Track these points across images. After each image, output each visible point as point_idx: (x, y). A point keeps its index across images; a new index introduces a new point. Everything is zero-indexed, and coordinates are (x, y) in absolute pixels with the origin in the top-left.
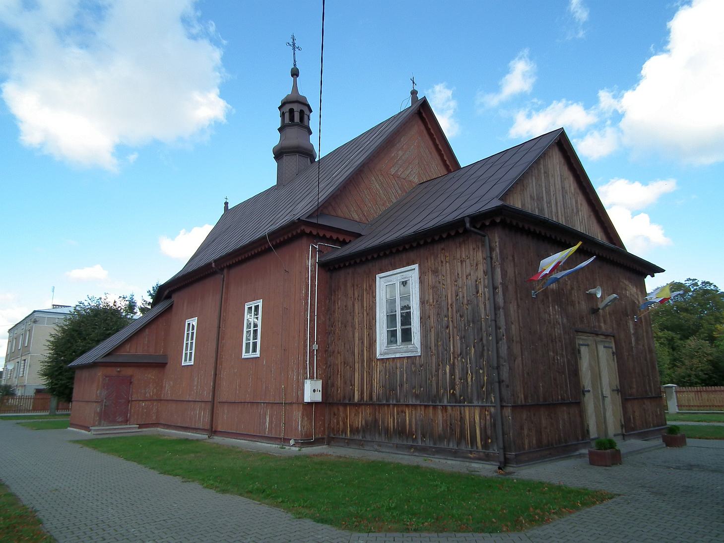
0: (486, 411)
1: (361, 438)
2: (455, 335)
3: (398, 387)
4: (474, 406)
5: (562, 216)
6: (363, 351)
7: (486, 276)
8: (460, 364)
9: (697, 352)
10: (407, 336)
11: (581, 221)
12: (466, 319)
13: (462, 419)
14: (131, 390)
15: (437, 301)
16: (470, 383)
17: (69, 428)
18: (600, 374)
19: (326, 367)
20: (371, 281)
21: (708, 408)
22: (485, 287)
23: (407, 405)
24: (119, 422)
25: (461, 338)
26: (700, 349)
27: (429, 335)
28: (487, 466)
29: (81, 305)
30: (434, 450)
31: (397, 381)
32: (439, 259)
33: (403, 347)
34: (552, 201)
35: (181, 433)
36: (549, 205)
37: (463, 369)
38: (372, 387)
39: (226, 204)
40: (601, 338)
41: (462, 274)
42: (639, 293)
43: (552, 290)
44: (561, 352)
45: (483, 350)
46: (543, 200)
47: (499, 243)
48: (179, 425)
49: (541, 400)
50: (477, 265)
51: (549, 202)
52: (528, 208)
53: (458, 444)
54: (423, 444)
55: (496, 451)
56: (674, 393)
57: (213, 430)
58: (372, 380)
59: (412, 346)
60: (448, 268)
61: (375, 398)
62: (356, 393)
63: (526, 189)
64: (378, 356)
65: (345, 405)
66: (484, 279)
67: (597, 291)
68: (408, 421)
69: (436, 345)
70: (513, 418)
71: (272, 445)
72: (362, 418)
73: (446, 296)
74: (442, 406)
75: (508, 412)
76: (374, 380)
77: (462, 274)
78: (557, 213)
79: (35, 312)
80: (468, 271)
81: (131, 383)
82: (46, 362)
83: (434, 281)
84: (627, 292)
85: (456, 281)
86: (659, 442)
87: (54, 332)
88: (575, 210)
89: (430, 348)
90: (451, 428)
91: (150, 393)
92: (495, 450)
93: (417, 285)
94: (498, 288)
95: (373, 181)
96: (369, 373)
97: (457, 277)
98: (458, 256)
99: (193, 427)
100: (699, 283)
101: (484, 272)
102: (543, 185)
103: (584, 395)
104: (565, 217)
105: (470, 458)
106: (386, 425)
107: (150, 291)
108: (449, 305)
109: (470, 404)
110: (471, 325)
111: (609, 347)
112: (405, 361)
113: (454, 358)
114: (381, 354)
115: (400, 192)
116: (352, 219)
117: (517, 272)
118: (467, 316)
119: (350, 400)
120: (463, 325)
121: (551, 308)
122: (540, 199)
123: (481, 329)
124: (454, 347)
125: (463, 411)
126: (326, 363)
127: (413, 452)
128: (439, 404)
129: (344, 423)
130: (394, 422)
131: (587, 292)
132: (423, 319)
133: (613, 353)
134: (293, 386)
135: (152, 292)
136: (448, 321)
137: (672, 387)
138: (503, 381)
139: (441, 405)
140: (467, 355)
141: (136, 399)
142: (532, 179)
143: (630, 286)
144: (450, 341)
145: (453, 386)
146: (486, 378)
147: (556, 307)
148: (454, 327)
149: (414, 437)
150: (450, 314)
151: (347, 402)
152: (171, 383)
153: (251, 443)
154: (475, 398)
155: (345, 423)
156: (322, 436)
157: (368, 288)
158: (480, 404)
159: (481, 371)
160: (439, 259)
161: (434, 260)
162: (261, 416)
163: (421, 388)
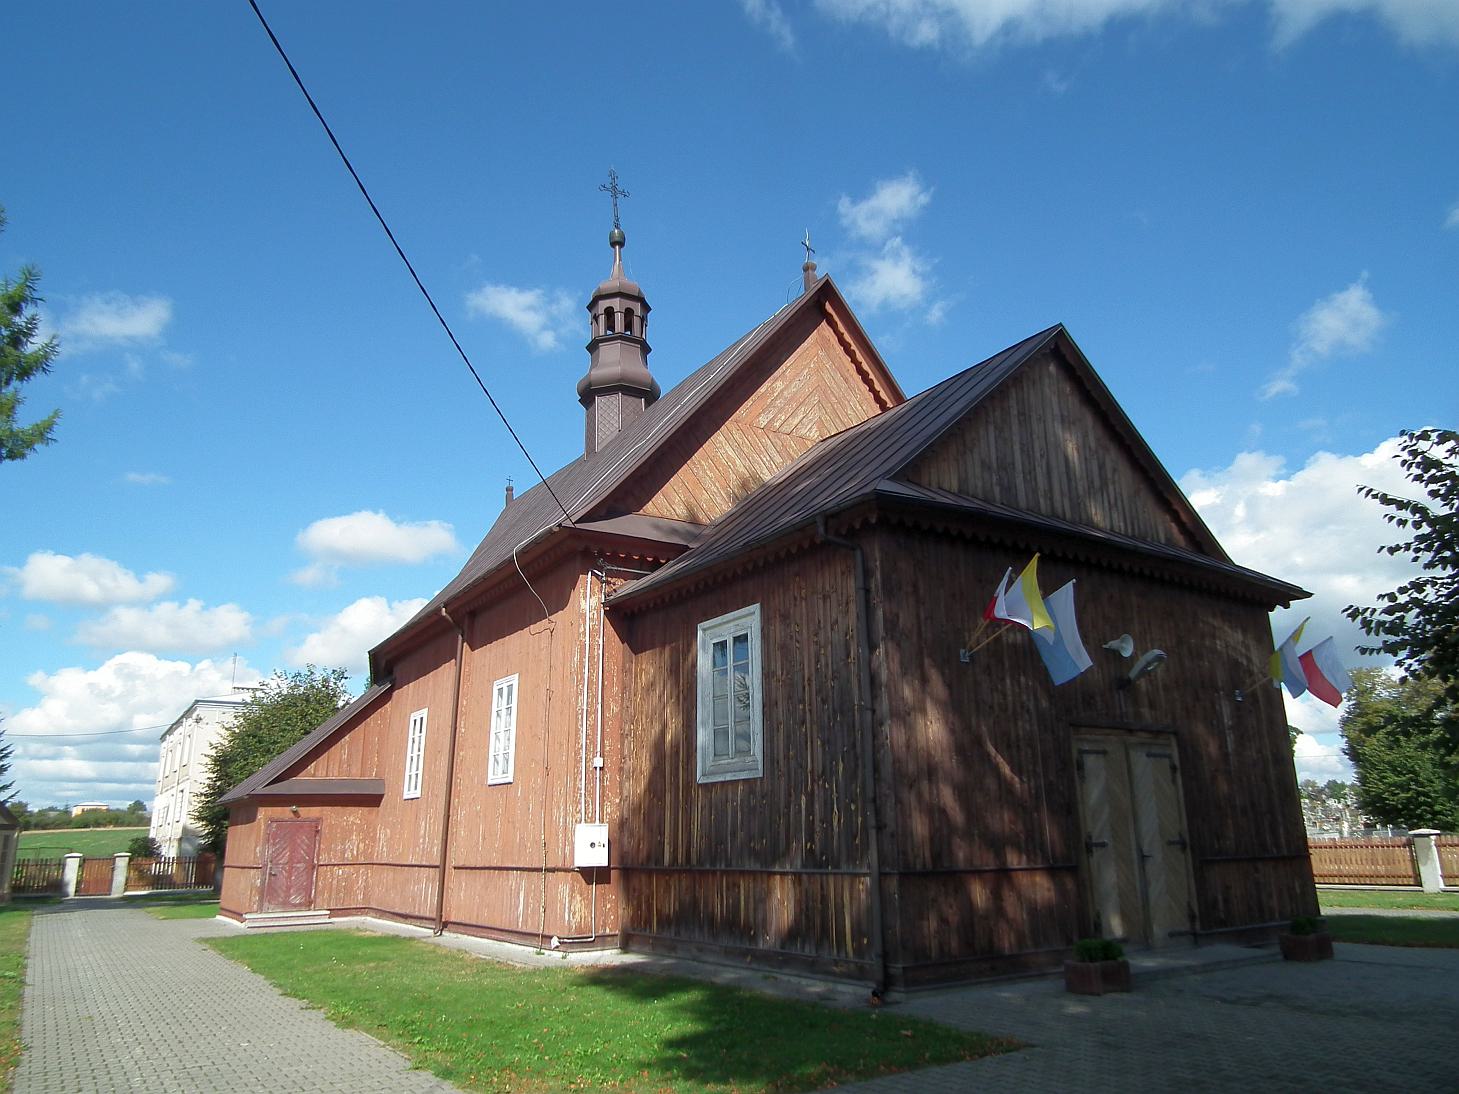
2: (815, 736)
4: (842, 874)
5: (1062, 494)
6: (677, 769)
11: (1112, 501)
12: (831, 707)
13: (824, 899)
15: (788, 674)
16: (836, 829)
17: (218, 917)
23: (742, 873)
24: (295, 906)
25: (823, 745)
29: (264, 687)
30: (780, 958)
34: (1038, 469)
36: (1028, 477)
39: (509, 490)
41: (825, 621)
42: (1251, 643)
43: (1014, 645)
44: (1031, 768)
45: (857, 766)
46: (1014, 468)
47: (881, 562)
48: (397, 910)
49: (694, 862)
52: (976, 487)
53: (819, 946)
56: (1434, 848)
57: (443, 920)
60: (804, 610)
62: (667, 847)
63: (972, 452)
64: (700, 779)
65: (650, 873)
67: (1124, 645)
68: (742, 903)
69: (787, 757)
70: (901, 897)
74: (794, 874)
77: (825, 621)
78: (1051, 489)
79: (197, 701)
81: (317, 832)
84: (1218, 642)
88: (1097, 483)
89: (778, 763)
90: (807, 916)
92: (873, 962)
95: (720, 442)
98: (820, 586)
102: (1016, 438)
103: (1089, 851)
104: (1071, 500)
105: (834, 974)
109: (836, 871)
111: (1165, 756)
112: (740, 787)
113: (813, 781)
114: (703, 775)
115: (778, 460)
116: (676, 518)
117: (922, 616)
121: (1008, 681)
123: (854, 727)
126: (621, 793)
127: (750, 963)
131: (1104, 646)
133: (1174, 768)
136: (804, 709)
137: (1428, 835)
140: (831, 777)
141: (326, 862)
142: (987, 430)
143: (1226, 628)
146: (860, 819)
149: (752, 933)
151: (654, 867)
152: (388, 831)
153: (496, 945)
154: (844, 858)
156: (611, 930)
158: (851, 870)
163: (762, 838)
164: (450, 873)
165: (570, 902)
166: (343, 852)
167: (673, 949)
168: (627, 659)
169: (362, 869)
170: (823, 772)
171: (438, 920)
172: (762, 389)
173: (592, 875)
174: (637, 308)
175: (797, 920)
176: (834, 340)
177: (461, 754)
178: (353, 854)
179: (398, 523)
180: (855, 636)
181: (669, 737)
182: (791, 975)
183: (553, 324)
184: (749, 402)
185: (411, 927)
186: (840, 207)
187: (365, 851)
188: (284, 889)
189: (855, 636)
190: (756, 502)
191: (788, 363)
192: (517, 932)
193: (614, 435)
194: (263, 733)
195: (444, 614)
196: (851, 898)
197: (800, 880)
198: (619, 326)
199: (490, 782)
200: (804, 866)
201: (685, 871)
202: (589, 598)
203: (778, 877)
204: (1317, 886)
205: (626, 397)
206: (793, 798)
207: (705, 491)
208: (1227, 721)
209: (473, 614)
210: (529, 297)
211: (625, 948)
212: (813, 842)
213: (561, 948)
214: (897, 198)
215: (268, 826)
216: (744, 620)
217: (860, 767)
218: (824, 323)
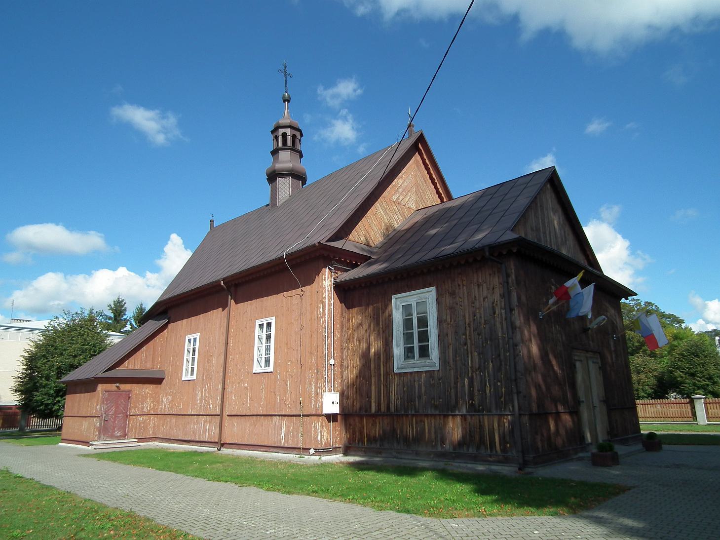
0: (504, 418)
1: (378, 446)
3: (417, 399)
4: (492, 415)
7: (502, 299)
8: (479, 377)
9: (644, 368)
10: (424, 352)
13: (481, 427)
14: (129, 405)
15: (455, 321)
17: (60, 444)
18: (591, 388)
19: (342, 381)
20: (386, 300)
21: (662, 419)
22: (501, 309)
25: (479, 354)
26: (646, 365)
27: (447, 351)
28: (506, 468)
30: (454, 455)
31: (415, 392)
32: (456, 283)
33: (422, 361)
35: (183, 446)
37: (481, 382)
38: (390, 398)
40: (590, 354)
42: (617, 314)
45: (501, 365)
47: (515, 270)
48: (180, 438)
50: (493, 289)
51: (545, 233)
53: (478, 448)
54: (443, 450)
55: (515, 454)
58: (389, 393)
59: (429, 361)
60: (465, 291)
61: (392, 409)
64: (396, 370)
66: (501, 302)
69: (455, 361)
71: (289, 455)
72: (379, 427)
73: (464, 316)
74: (461, 415)
75: (525, 419)
76: (392, 392)
80: (485, 294)
81: (129, 397)
82: (19, 377)
83: (451, 302)
85: (473, 303)
86: (640, 446)
87: (27, 347)
89: (449, 363)
91: (147, 408)
93: (435, 306)
94: (514, 310)
96: (386, 386)
97: (474, 299)
98: (475, 280)
99: (197, 439)
100: (642, 303)
101: (500, 295)
103: (580, 404)
106: (405, 433)
107: (110, 305)
108: (467, 324)
110: (489, 343)
112: (423, 375)
113: (473, 372)
114: (398, 369)
115: (401, 218)
118: (485, 334)
119: (366, 411)
120: (481, 342)
122: (538, 230)
124: (472, 361)
125: (482, 420)
128: (458, 413)
129: (361, 434)
130: (413, 431)
132: (441, 336)
134: (311, 398)
135: (113, 306)
136: (466, 339)
137: (701, 398)
138: (520, 392)
139: (460, 415)
144: (468, 357)
145: (472, 398)
146: (503, 389)
147: (557, 327)
148: (471, 344)
150: (468, 332)
151: (364, 413)
153: (266, 454)
155: (361, 433)
157: (383, 308)
158: (499, 413)
159: (499, 384)
160: (456, 283)
161: (451, 284)
162: (276, 427)
164: (226, 420)
165: (321, 431)
166: (143, 408)
167: (380, 453)
168: (344, 311)
169: (152, 417)
170: (479, 368)
171: (219, 443)
172: (394, 183)
173: (331, 418)
174: (298, 134)
175: (464, 437)
176: (421, 162)
177: (231, 357)
178: (147, 409)
179: (71, 231)
180: (499, 304)
181: (373, 350)
182: (461, 463)
183: (165, 130)
184: (389, 189)
185: (193, 447)
186: (318, 90)
187: (154, 408)
188: (112, 428)
189: (499, 304)
190: (396, 240)
191: (403, 171)
192: (280, 447)
193: (287, 198)
194: (58, 344)
195: (222, 284)
196: (499, 426)
197: (465, 420)
198: (289, 143)
199: (254, 371)
200: (467, 411)
201: (387, 415)
202: (326, 279)
203: (451, 417)
204: (640, 422)
205: (293, 179)
206: (459, 380)
207: (370, 232)
208: (613, 349)
209: (237, 286)
210: (150, 114)
211: (346, 453)
212: (473, 400)
213: (316, 454)
214: (347, 88)
215: (103, 395)
216: (424, 294)
217: (503, 365)
218: (417, 153)
